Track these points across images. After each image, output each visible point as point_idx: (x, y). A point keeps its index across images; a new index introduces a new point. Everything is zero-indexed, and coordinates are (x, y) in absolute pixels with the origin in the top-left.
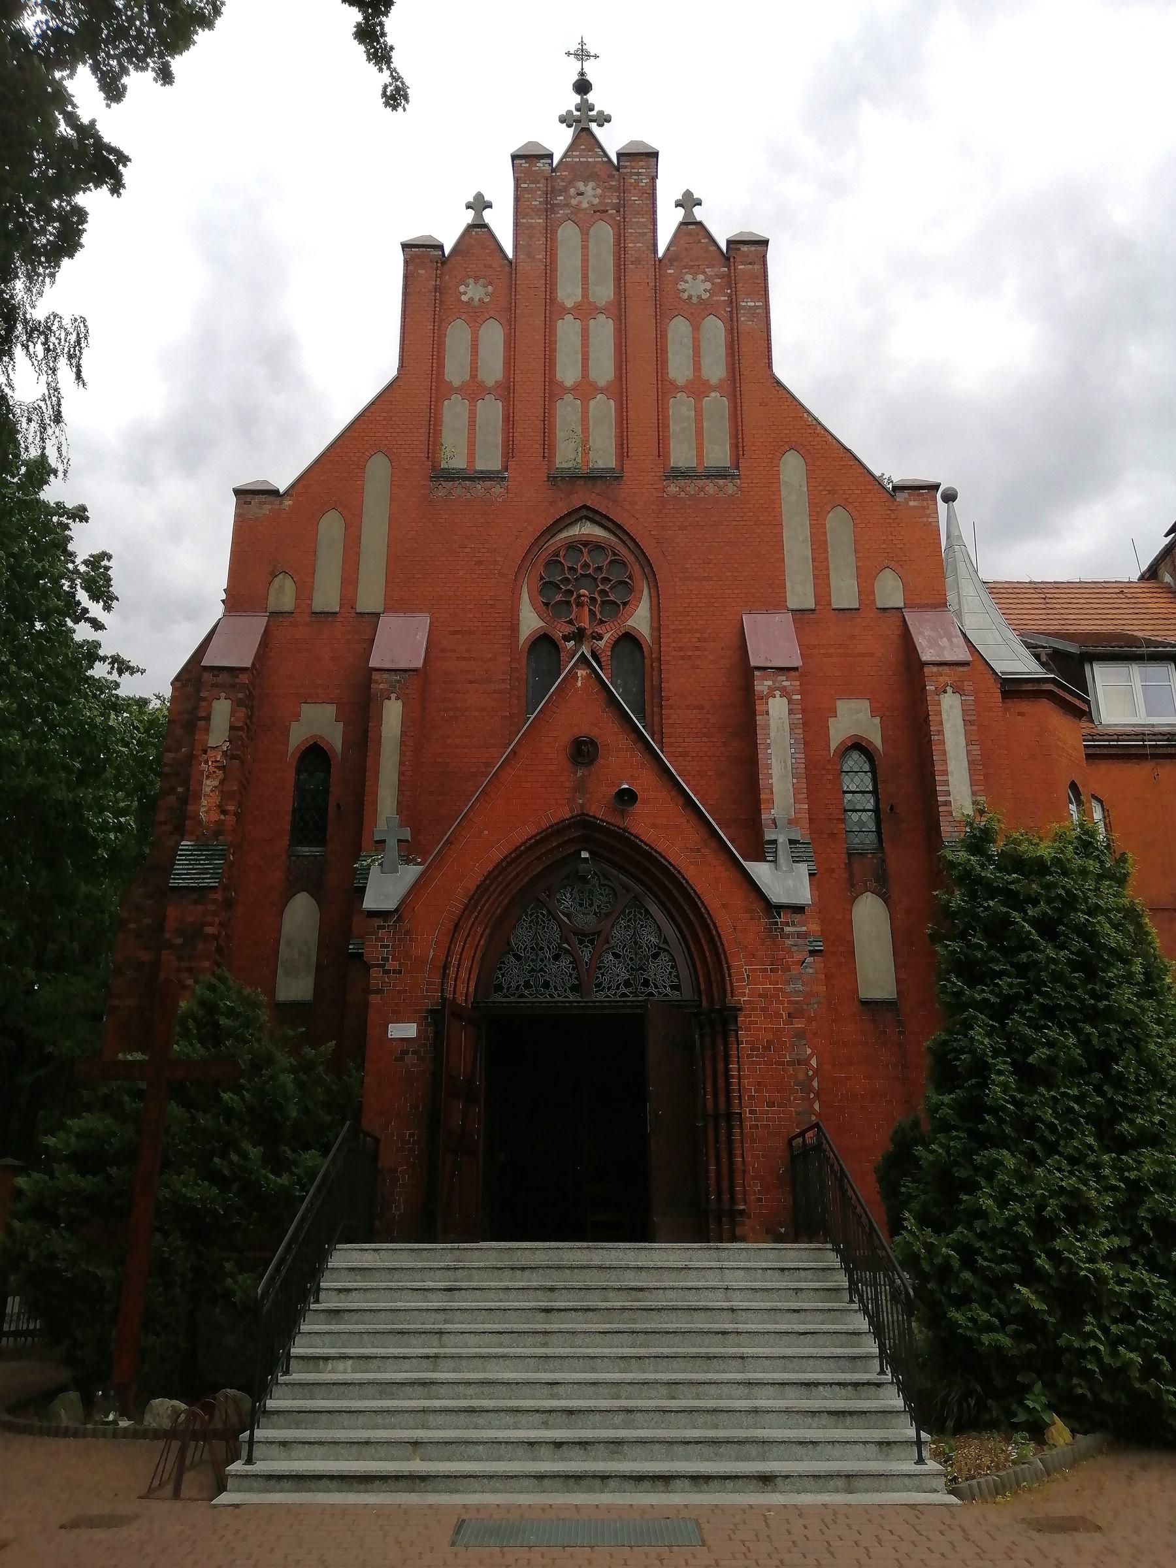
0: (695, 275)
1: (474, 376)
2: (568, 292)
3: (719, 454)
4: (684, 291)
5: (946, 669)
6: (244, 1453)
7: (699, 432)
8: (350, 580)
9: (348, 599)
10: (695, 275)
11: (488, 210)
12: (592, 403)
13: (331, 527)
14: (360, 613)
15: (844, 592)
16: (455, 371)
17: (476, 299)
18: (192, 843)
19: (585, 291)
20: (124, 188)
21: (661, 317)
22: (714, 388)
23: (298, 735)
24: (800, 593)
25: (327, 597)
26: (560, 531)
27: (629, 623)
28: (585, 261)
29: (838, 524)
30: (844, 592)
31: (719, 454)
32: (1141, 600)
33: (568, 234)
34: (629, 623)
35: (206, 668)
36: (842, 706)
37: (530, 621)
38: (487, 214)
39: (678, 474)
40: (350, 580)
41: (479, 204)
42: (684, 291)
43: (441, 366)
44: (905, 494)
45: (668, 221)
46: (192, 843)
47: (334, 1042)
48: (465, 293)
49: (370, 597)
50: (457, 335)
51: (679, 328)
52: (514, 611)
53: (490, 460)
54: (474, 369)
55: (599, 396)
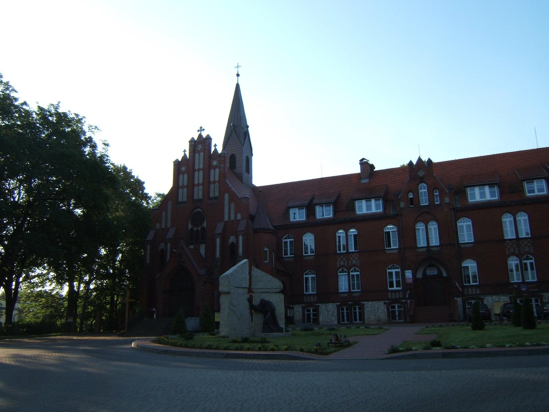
0: (215, 161)
1: (183, 184)
2: (197, 167)
3: (217, 194)
5: (240, 232)
8: (166, 223)
9: (166, 226)
10: (215, 161)
15: (233, 218)
16: (181, 184)
19: (199, 166)
20: (193, 138)
21: (210, 170)
22: (217, 182)
23: (160, 248)
24: (226, 219)
25: (163, 226)
29: (233, 205)
30: (233, 218)
31: (217, 194)
32: (399, 185)
33: (197, 155)
36: (231, 237)
37: (190, 226)
38: (216, 147)
39: (212, 199)
40: (166, 223)
41: (185, 151)
42: (182, 169)
43: (194, 181)
44: (242, 199)
45: (213, 149)
47: (252, 266)
49: (169, 226)
50: (181, 176)
51: (212, 171)
52: (188, 226)
53: (185, 200)
54: (183, 183)
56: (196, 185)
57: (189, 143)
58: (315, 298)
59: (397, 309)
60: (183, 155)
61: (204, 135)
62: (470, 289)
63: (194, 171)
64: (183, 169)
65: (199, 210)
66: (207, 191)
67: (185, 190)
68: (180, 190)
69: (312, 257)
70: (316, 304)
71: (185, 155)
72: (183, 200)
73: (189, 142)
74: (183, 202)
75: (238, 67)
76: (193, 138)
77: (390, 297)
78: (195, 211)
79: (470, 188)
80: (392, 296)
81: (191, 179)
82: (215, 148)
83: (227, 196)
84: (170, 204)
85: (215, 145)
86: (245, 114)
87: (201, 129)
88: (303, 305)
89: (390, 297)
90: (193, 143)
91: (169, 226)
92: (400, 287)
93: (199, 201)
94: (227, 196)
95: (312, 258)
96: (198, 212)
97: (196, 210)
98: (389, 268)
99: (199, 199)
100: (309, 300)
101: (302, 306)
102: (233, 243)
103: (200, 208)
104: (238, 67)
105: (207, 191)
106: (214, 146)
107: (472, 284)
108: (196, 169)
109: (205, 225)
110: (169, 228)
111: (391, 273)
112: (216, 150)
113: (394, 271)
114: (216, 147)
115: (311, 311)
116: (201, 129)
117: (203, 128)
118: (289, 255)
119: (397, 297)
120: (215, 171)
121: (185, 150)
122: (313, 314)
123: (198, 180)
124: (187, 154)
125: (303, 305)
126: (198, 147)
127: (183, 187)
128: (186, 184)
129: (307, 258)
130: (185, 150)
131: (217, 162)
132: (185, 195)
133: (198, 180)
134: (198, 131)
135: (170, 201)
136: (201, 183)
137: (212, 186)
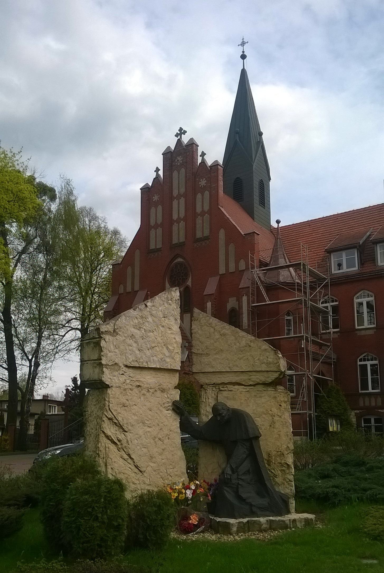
1: (156, 222)
2: (175, 193)
3: (207, 233)
4: (200, 185)
6: (291, 521)
7: (203, 227)
9: (133, 288)
11: (159, 171)
12: (180, 223)
13: (129, 269)
14: (241, 271)
15: (232, 268)
16: (152, 223)
17: (156, 200)
18: (303, 341)
19: (179, 191)
20: (169, 147)
24: (222, 270)
25: (129, 289)
26: (173, 262)
27: (187, 284)
28: (179, 182)
29: (232, 248)
31: (207, 233)
33: (175, 174)
34: (187, 284)
35: (240, 289)
36: (230, 300)
41: (157, 170)
46: (303, 341)
48: (154, 199)
50: (153, 210)
51: (199, 196)
53: (159, 246)
55: (206, 215)
56: (175, 221)
57: (162, 156)
58: (379, 400)
59: (374, 425)
60: (154, 175)
61: (185, 139)
62: (367, 399)
63: (172, 198)
64: (156, 198)
65: (180, 260)
66: (168, 234)
67: (160, 231)
68: (152, 232)
69: (371, 331)
70: (380, 411)
71: (158, 175)
72: (156, 246)
73: (162, 154)
74: (157, 250)
75: (243, 44)
76: (169, 147)
77: (361, 404)
78: (175, 262)
79: (335, 253)
80: (370, 403)
81: (168, 212)
82: (203, 159)
83: (222, 234)
84: (137, 253)
85: (203, 154)
86: (253, 99)
87: (182, 132)
88: (358, 412)
89: (361, 404)
90: (169, 155)
91: (137, 288)
92: (294, 393)
93: (181, 245)
94: (222, 234)
95: (371, 332)
96: (179, 263)
97: (176, 261)
98: (361, 359)
99: (180, 243)
100: (367, 404)
101: (355, 413)
102: (233, 310)
103: (184, 258)
104: (243, 44)
105: (168, 234)
106: (160, 170)
107: (370, 390)
108: (175, 196)
109: (189, 283)
110: (138, 291)
111: (364, 368)
112: (203, 162)
113: (369, 363)
114: (205, 157)
115: (372, 423)
116: (182, 132)
117: (184, 129)
118: (366, 325)
119: (373, 404)
120: (203, 195)
121: (157, 168)
122: (376, 427)
123: (203, 206)
124: (161, 173)
125: (358, 412)
126: (176, 160)
127: (156, 226)
128: (160, 220)
129: (363, 333)
130: (157, 168)
131: (206, 181)
132: (160, 239)
133: (203, 206)
134: (176, 136)
135: (138, 250)
136: (206, 211)
137: (199, 221)
